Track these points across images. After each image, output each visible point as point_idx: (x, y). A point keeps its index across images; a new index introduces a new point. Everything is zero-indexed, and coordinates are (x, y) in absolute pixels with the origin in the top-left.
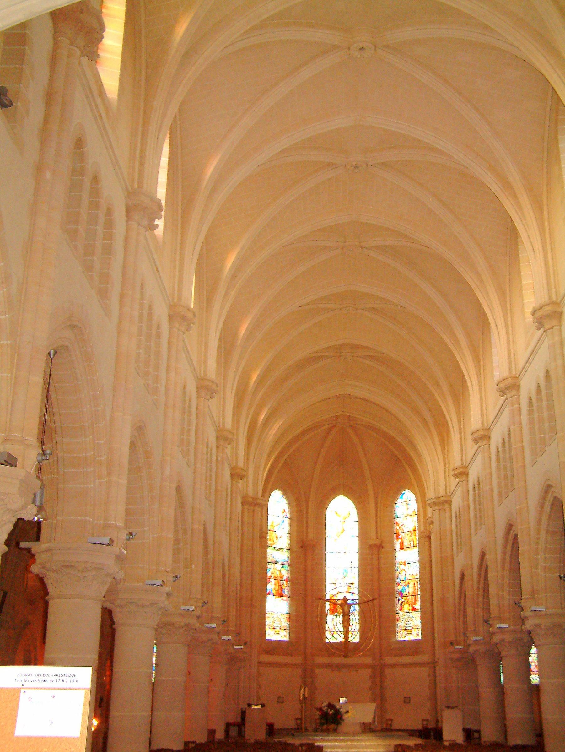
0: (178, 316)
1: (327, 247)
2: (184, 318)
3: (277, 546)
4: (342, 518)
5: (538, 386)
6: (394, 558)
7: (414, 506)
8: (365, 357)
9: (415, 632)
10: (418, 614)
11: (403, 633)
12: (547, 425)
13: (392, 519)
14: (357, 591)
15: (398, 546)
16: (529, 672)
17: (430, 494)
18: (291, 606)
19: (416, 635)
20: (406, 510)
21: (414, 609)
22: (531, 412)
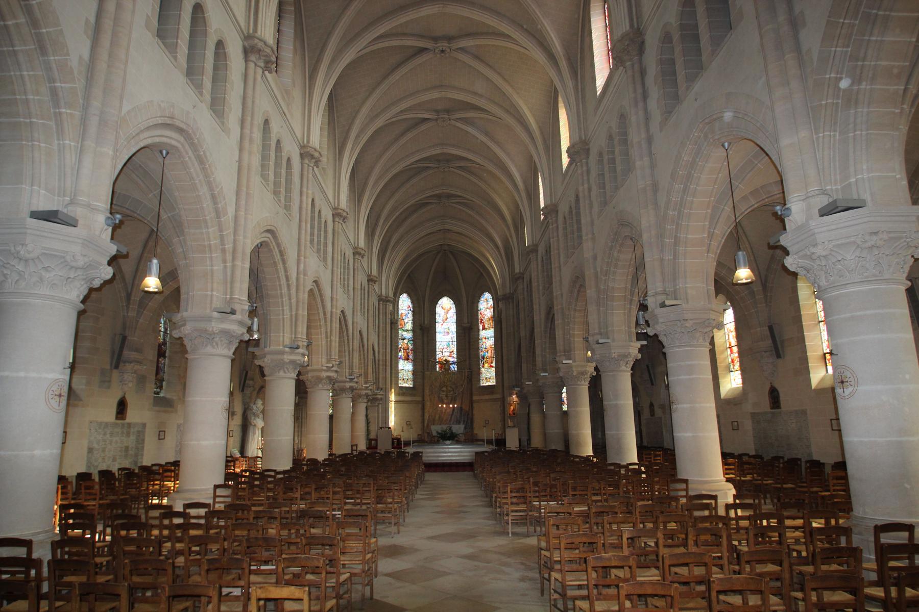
2: (312, 157)
6: (478, 335)
7: (491, 302)
12: (576, 234)
15: (481, 328)
16: (562, 403)
18: (414, 366)
19: (492, 382)
20: (486, 306)
22: (565, 228)
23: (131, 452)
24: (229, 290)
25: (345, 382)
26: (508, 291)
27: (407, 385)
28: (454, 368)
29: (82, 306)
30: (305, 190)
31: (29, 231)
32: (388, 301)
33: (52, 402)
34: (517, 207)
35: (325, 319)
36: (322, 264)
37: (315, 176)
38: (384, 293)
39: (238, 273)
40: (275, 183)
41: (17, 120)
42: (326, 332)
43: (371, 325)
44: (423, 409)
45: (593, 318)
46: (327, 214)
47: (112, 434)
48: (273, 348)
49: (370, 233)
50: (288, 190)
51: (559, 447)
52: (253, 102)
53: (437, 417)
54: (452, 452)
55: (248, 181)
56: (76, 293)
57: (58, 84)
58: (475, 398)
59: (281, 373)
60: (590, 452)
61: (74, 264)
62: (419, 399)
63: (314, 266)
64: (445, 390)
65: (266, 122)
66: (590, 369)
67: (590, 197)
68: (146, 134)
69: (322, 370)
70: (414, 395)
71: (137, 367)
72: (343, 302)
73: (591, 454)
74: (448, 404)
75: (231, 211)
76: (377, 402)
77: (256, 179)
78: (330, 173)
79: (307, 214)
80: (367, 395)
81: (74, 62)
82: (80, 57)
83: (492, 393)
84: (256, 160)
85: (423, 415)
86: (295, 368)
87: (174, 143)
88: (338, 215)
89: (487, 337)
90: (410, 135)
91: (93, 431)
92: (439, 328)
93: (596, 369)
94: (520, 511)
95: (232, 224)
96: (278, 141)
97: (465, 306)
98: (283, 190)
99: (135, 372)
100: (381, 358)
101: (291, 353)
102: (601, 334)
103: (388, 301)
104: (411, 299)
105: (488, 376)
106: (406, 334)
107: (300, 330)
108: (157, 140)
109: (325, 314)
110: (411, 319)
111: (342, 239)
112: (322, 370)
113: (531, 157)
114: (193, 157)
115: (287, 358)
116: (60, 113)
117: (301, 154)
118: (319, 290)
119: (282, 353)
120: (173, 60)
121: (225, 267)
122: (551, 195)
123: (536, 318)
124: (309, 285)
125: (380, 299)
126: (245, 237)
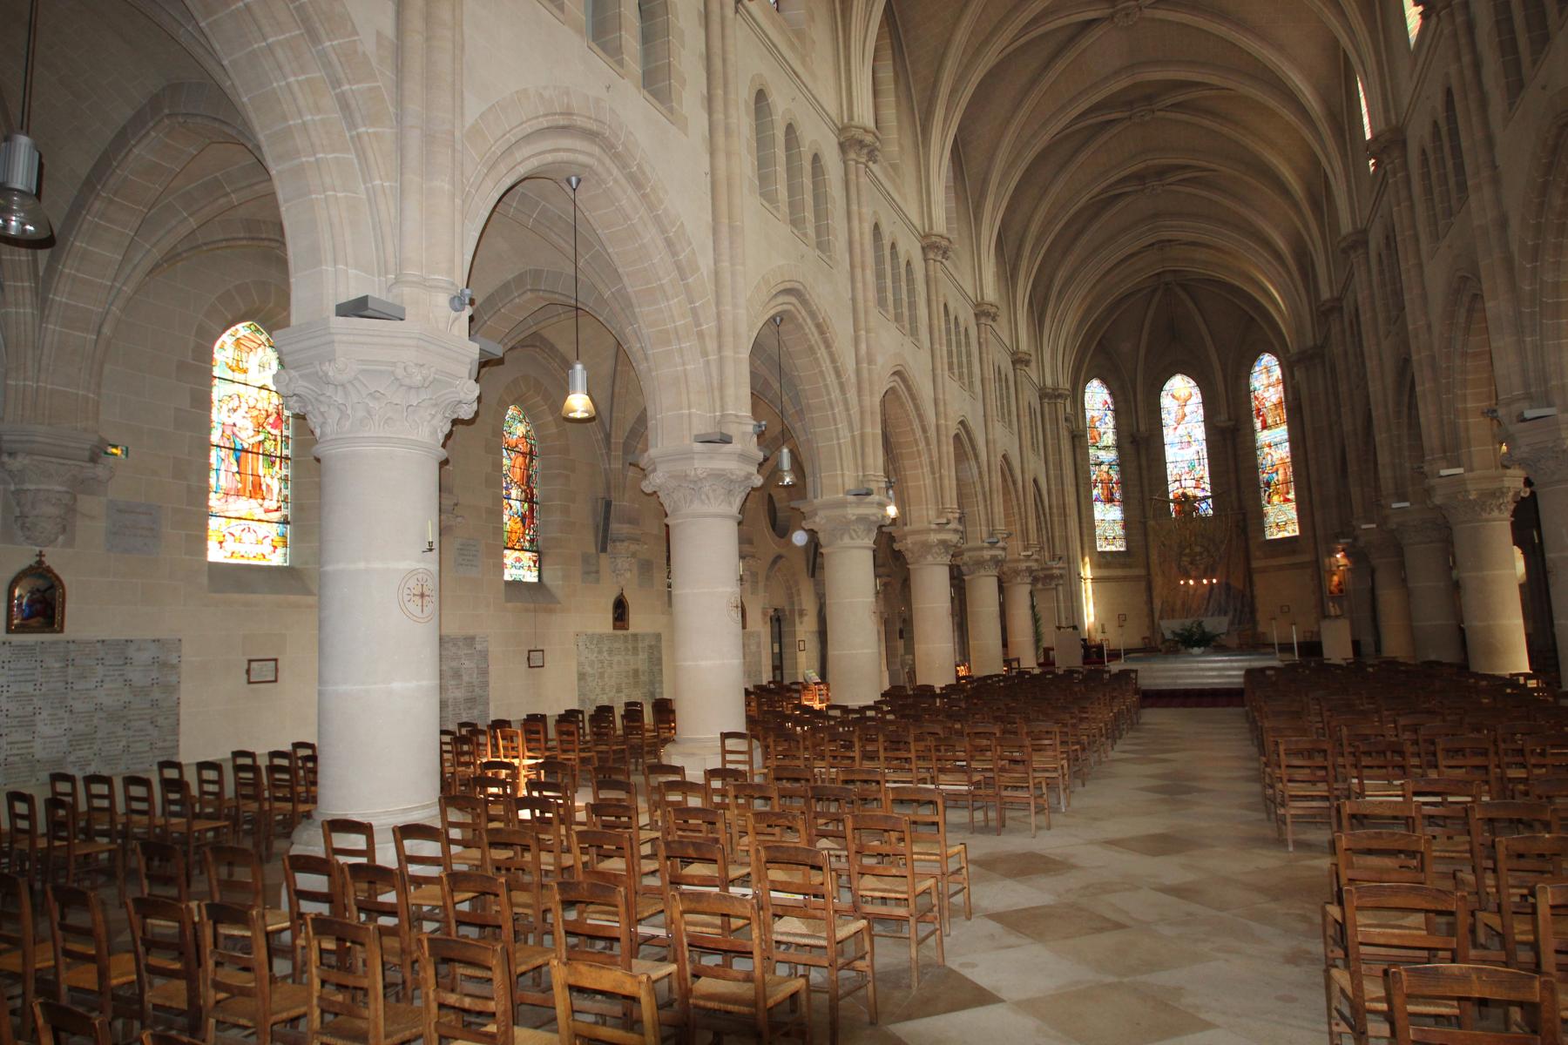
1: (1094, 20)
3: (1100, 445)
4: (1181, 401)
5: (1435, 124)
6: (1254, 441)
7: (1277, 373)
9: (1290, 528)
10: (1293, 505)
13: (1248, 392)
14: (1208, 487)
15: (1258, 425)
18: (1124, 511)
19: (1293, 530)
20: (1266, 381)
23: (644, 678)
24: (718, 404)
25: (982, 549)
26: (1310, 343)
27: (1113, 548)
28: (1206, 509)
29: (443, 454)
30: (854, 207)
31: (337, 338)
32: (1060, 396)
33: (411, 606)
34: (1315, 162)
35: (927, 439)
36: (908, 340)
37: (876, 181)
38: (1049, 382)
39: (729, 370)
40: (792, 205)
41: (296, 162)
42: (931, 463)
43: (1027, 442)
44: (1149, 589)
45: (1507, 364)
46: (910, 248)
47: (610, 652)
48: (827, 497)
49: (1008, 275)
50: (821, 213)
51: (1448, 656)
52: (724, 60)
53: (1179, 603)
54: (1218, 669)
55: (730, 204)
56: (428, 430)
57: (346, 87)
58: (1255, 564)
59: (847, 540)
60: (1522, 665)
61: (407, 381)
62: (1142, 572)
63: (889, 345)
64: (1197, 555)
65: (761, 96)
66: (1514, 481)
67: (1479, 83)
68: (527, 151)
69: (929, 531)
70: (1130, 567)
71: (633, 547)
72: (959, 404)
73: (1526, 669)
74: (1198, 579)
75: (705, 263)
76: (1053, 581)
77: (748, 203)
78: (908, 168)
79: (863, 251)
80: (1030, 571)
81: (368, 45)
82: (379, 34)
83: (1294, 552)
84: (745, 165)
85: (1150, 601)
86: (870, 530)
87: (582, 158)
88: (932, 247)
89: (1274, 444)
90: (1060, 65)
91: (582, 648)
92: (1169, 435)
93: (1528, 482)
94: (1313, 798)
95: (710, 287)
96: (790, 128)
97: (1221, 387)
98: (809, 215)
99: (634, 555)
100: (1054, 502)
101: (858, 504)
102: (1529, 397)
103: (1060, 396)
104: (1108, 388)
105: (1282, 519)
106: (1104, 453)
107: (870, 461)
108: (549, 158)
109: (924, 430)
110: (1111, 425)
111: (947, 291)
112: (929, 531)
113: (1336, 41)
114: (623, 181)
115: (853, 512)
116: (359, 136)
117: (841, 145)
118: (909, 388)
119: (843, 504)
120: (556, 11)
121: (708, 362)
122: (1386, 111)
123: (1374, 388)
124: (883, 383)
125: (1044, 394)
126: (735, 306)
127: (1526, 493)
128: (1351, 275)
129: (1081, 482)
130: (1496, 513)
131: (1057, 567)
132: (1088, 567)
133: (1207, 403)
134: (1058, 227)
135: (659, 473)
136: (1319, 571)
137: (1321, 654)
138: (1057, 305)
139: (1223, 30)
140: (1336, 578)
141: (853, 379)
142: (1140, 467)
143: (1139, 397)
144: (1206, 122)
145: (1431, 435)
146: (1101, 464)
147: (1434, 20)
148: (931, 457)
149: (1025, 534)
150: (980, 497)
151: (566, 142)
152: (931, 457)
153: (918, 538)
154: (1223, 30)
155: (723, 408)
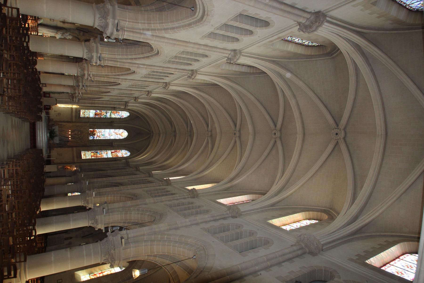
0: (193, 73)
1: (208, 126)
2: (192, 75)
3: (112, 114)
4: (121, 134)
5: (169, 191)
6: (109, 150)
7: (125, 156)
8: (172, 139)
10: (91, 158)
11: (84, 153)
14: (97, 138)
15: (112, 151)
17: (130, 160)
18: (92, 118)
19: (83, 157)
20: (124, 153)
21: (92, 156)
22: (160, 189)
26: (130, 164)
27: (81, 114)
28: (91, 138)
32: (126, 106)
35: (116, 75)
37: (184, 76)
38: (129, 104)
42: (109, 75)
43: (113, 97)
46: (167, 80)
48: (100, 48)
53: (64, 129)
54: (42, 137)
58: (75, 149)
62: (74, 120)
63: (142, 72)
65: (207, 56)
70: (76, 117)
72: (124, 84)
73: (42, 210)
75: (167, 36)
78: (186, 83)
80: (75, 93)
83: (77, 157)
86: (89, 58)
87: (197, 14)
88: (166, 85)
89: (107, 154)
90: (201, 119)
92: (112, 131)
93: (90, 209)
101: (97, 57)
102: (108, 209)
103: (126, 106)
104: (127, 117)
105: (87, 155)
106: (109, 114)
107: (110, 62)
110: (117, 117)
117: (193, 70)
118: (130, 74)
119: (97, 52)
121: (140, 30)
122: (175, 182)
123: (117, 178)
124: (133, 69)
125: (126, 103)
127: (87, 208)
128: (144, 173)
129: (102, 108)
130: (83, 203)
131: (76, 100)
132: (76, 107)
133: (120, 140)
134: (167, 112)
135: (110, 7)
136: (72, 163)
137: (47, 164)
138: (150, 109)
139: (200, 152)
140: (69, 167)
141: (133, 62)
142: (104, 123)
143: (123, 124)
144: (183, 146)
145: (102, 190)
146: (106, 113)
147: (188, 192)
148: (110, 75)
149: (85, 94)
150: (98, 85)
151: (200, 14)
152: (110, 75)
153: (86, 68)
154: (200, 152)
155: (127, 31)
